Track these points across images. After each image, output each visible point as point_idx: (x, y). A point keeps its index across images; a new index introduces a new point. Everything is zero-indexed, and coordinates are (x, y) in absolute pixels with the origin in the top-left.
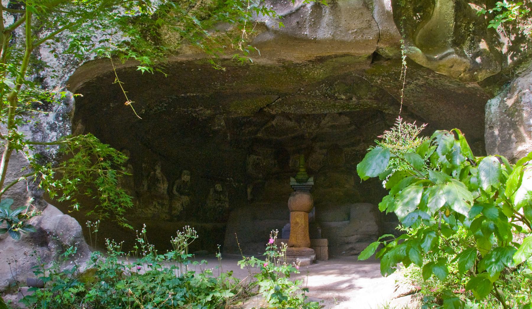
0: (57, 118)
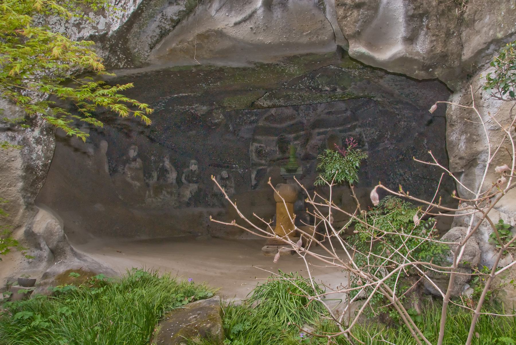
0: (41, 132)
